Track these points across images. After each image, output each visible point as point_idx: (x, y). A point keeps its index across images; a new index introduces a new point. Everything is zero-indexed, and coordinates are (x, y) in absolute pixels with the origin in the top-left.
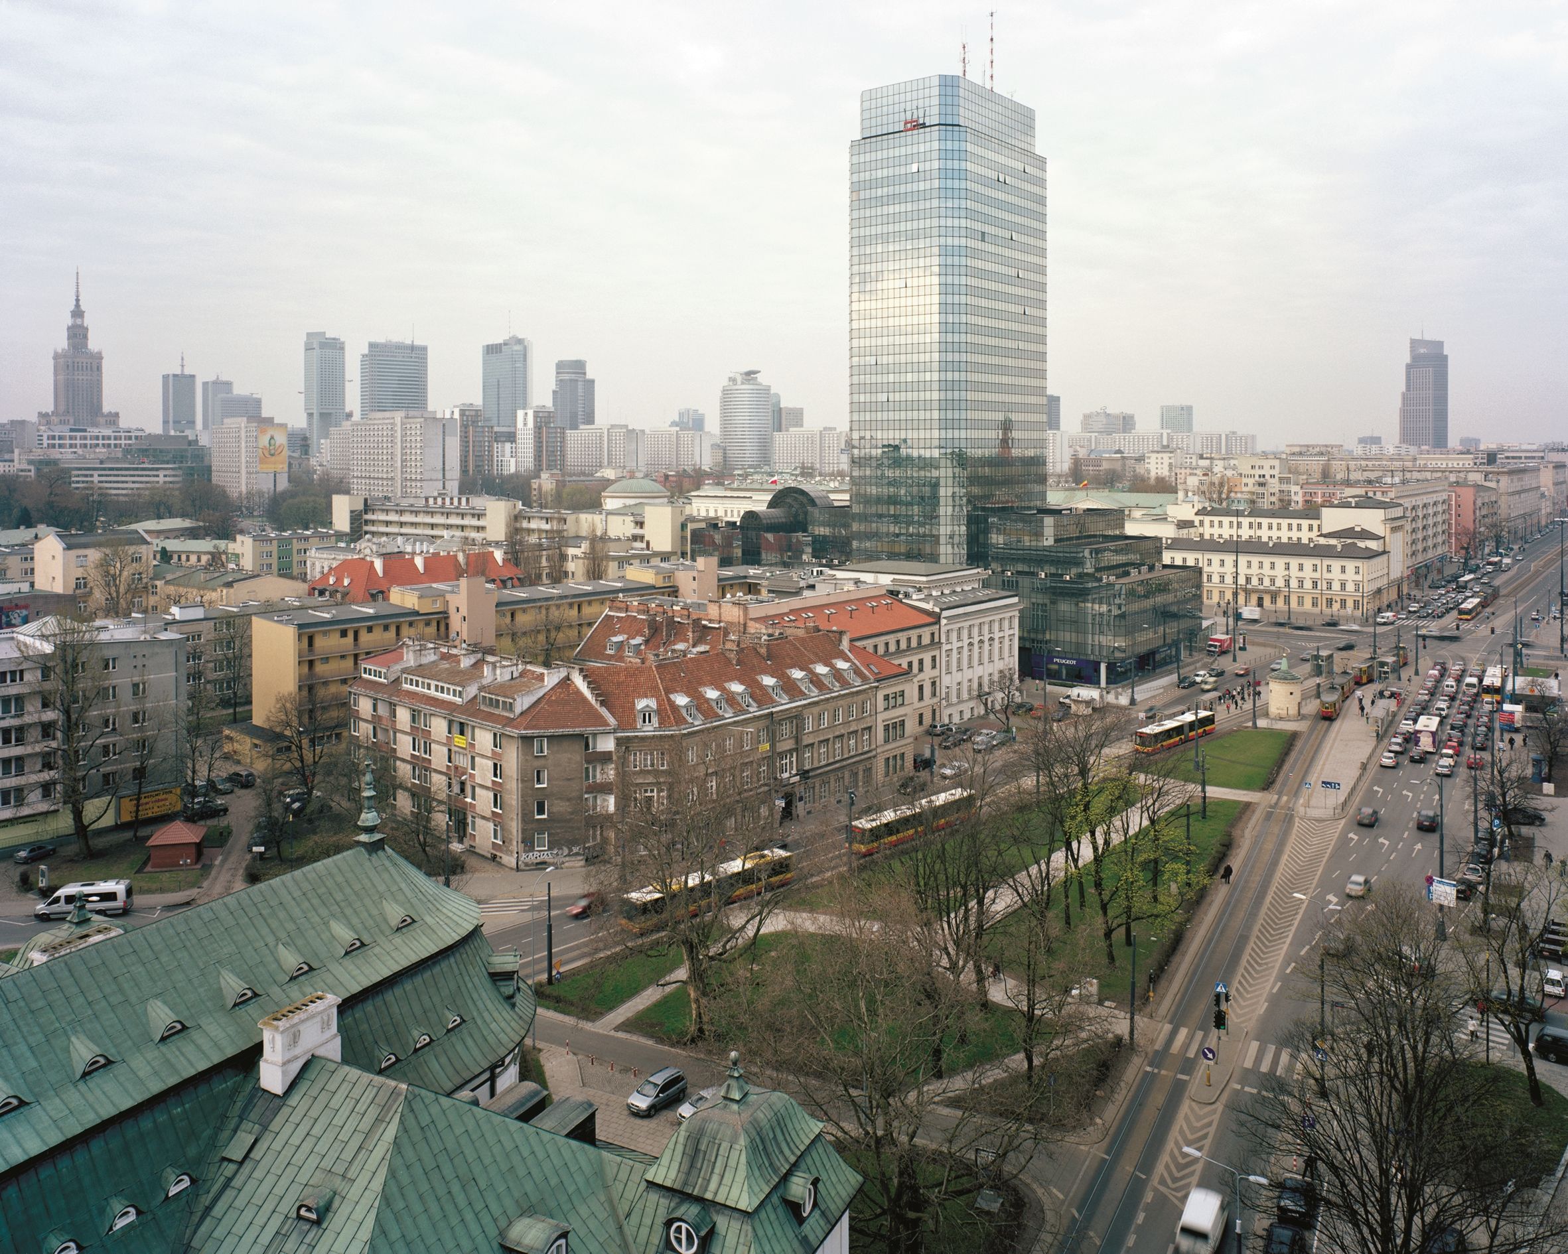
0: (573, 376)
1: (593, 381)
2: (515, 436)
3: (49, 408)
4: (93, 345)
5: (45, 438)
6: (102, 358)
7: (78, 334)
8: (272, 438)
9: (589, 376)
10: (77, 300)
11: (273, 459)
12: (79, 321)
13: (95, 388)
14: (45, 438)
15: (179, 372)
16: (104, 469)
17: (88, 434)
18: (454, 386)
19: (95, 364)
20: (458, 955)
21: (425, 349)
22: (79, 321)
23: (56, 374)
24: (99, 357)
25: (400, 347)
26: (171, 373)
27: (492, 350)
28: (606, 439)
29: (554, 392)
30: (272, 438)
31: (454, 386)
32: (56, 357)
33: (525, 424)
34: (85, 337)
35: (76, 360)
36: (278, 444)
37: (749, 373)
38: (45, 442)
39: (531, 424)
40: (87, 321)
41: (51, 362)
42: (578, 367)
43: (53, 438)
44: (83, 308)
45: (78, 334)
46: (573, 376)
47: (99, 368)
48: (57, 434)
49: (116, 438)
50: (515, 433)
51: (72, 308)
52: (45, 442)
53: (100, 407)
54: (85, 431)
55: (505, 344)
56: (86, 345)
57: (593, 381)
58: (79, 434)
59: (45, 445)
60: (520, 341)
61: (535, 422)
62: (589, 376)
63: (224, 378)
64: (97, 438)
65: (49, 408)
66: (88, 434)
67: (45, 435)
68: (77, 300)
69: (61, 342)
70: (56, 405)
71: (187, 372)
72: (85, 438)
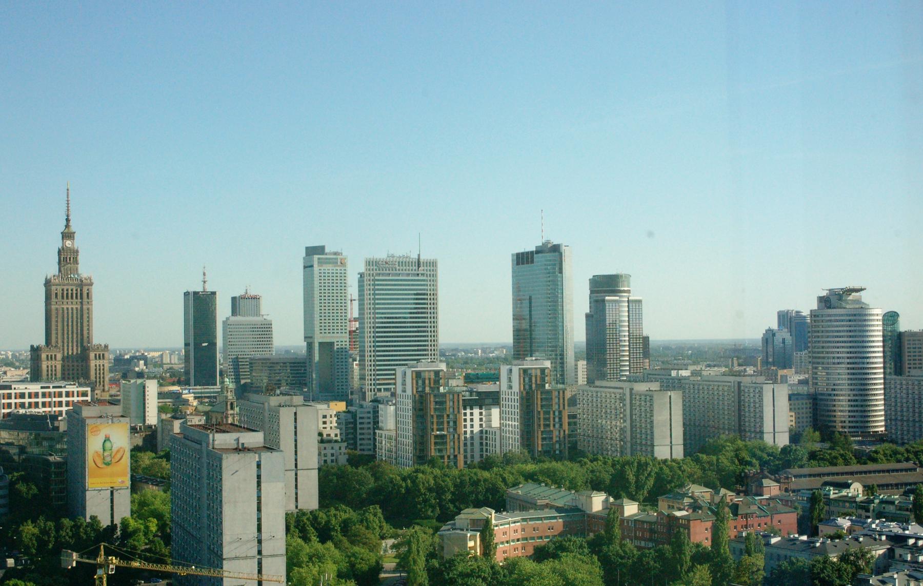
8: (107, 439)
10: (68, 220)
11: (109, 469)
13: (82, 320)
15: (199, 289)
17: (13, 391)
19: (81, 292)
20: (808, 410)
21: (433, 264)
22: (68, 243)
25: (404, 262)
26: (191, 290)
27: (522, 259)
29: (587, 316)
30: (107, 439)
36: (115, 449)
40: (78, 243)
44: (73, 229)
49: (44, 395)
51: (62, 228)
63: (252, 293)
64: (22, 396)
66: (13, 391)
68: (68, 220)
71: (209, 289)
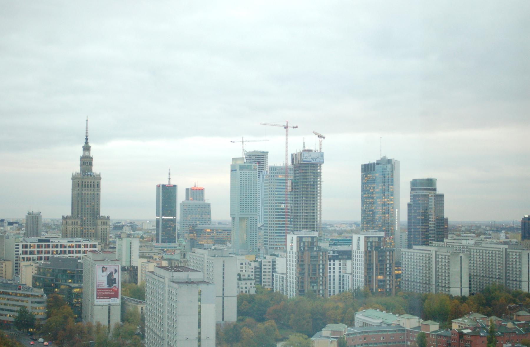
0: (425, 192)
1: (442, 196)
2: (351, 255)
3: (68, 212)
4: (96, 169)
5: (20, 247)
6: (100, 179)
7: (86, 162)
12: (87, 153)
13: (96, 198)
14: (20, 247)
17: (51, 244)
18: (339, 198)
22: (87, 153)
23: (73, 190)
24: (99, 178)
28: (434, 259)
29: (409, 205)
31: (339, 198)
32: (74, 178)
34: (91, 164)
35: (84, 180)
38: (21, 250)
41: (71, 181)
43: (26, 246)
45: (86, 162)
46: (425, 192)
47: (98, 186)
48: (29, 244)
50: (351, 251)
51: (83, 144)
52: (21, 250)
53: (98, 213)
54: (49, 241)
55: (378, 164)
56: (91, 170)
57: (442, 196)
58: (43, 244)
59: (20, 252)
60: (389, 161)
62: (439, 191)
64: (57, 246)
66: (51, 244)
67: (21, 245)
69: (77, 169)
70: (72, 214)
71: (172, 183)
72: (48, 246)
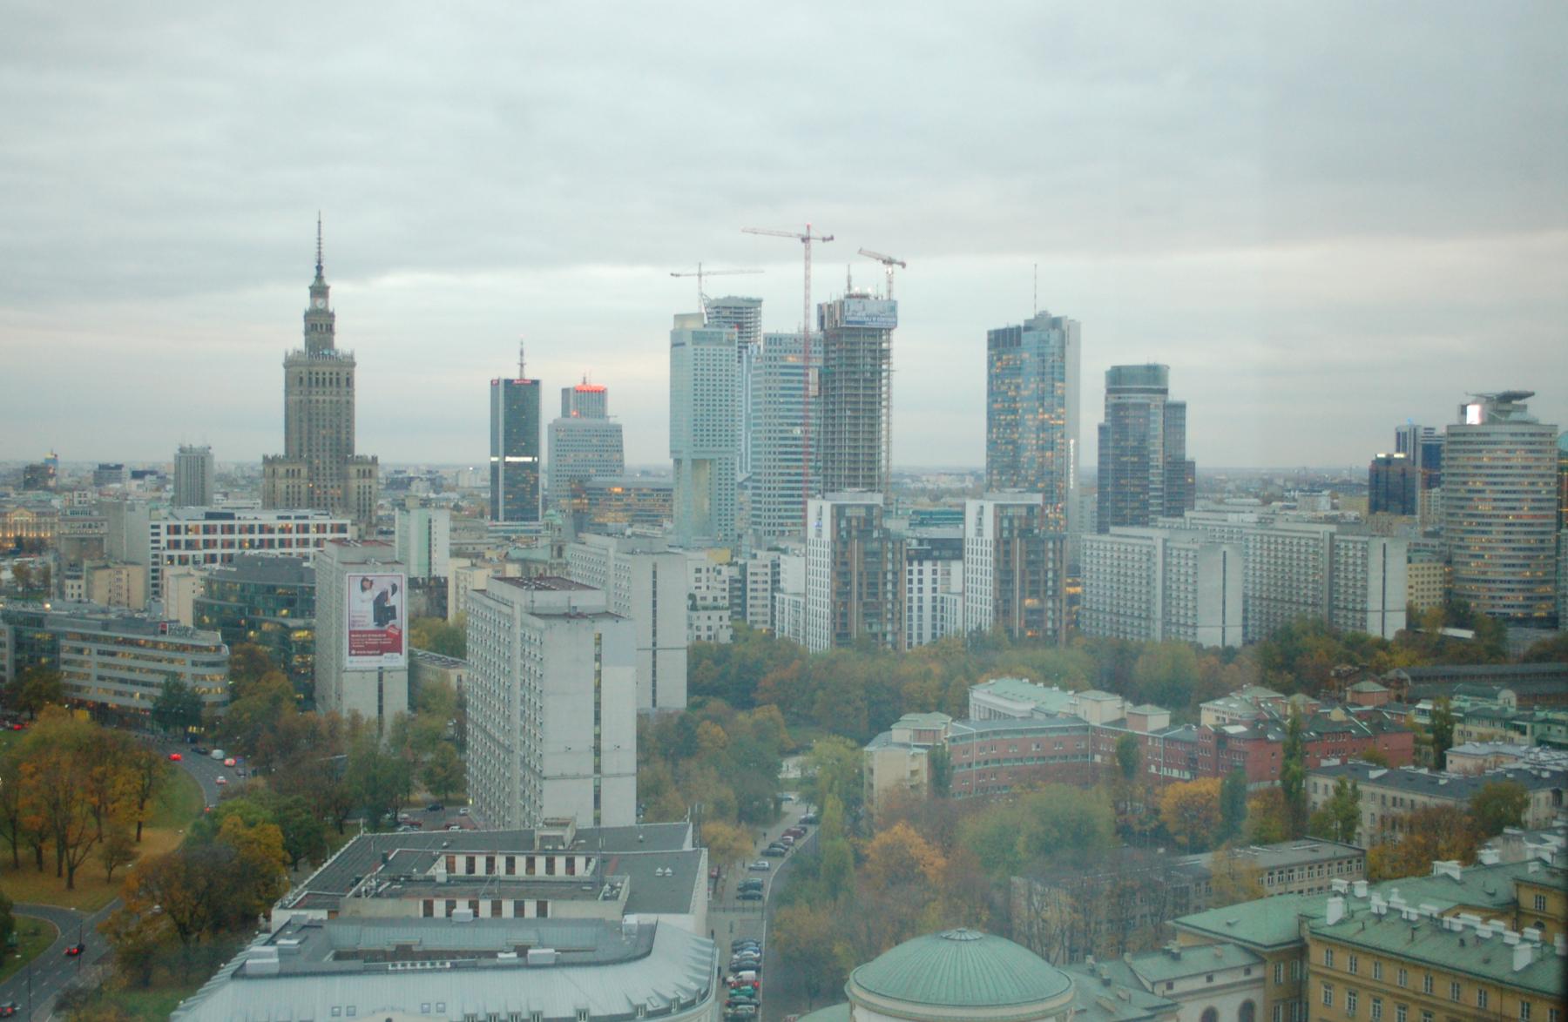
1: (1180, 407)
3: (277, 447)
4: (342, 342)
6: (353, 365)
7: (319, 324)
9: (1174, 395)
10: (319, 268)
12: (320, 303)
14: (163, 530)
16: (106, 640)
17: (235, 523)
22: (320, 303)
23: (288, 392)
27: (1003, 341)
28: (1159, 559)
29: (1102, 429)
32: (290, 364)
33: (980, 532)
34: (330, 329)
35: (314, 369)
37: (1507, 398)
38: (164, 538)
39: (989, 533)
41: (282, 372)
42: (1153, 376)
43: (177, 530)
45: (319, 324)
47: (349, 382)
48: (182, 523)
51: (312, 281)
52: (164, 538)
54: (231, 516)
55: (1028, 328)
56: (330, 345)
57: (1180, 407)
58: (219, 523)
59: (164, 544)
60: (1056, 323)
61: (999, 529)
62: (1174, 395)
65: (277, 447)
66: (235, 523)
68: (319, 268)
69: (296, 341)
71: (530, 375)
72: (231, 529)
